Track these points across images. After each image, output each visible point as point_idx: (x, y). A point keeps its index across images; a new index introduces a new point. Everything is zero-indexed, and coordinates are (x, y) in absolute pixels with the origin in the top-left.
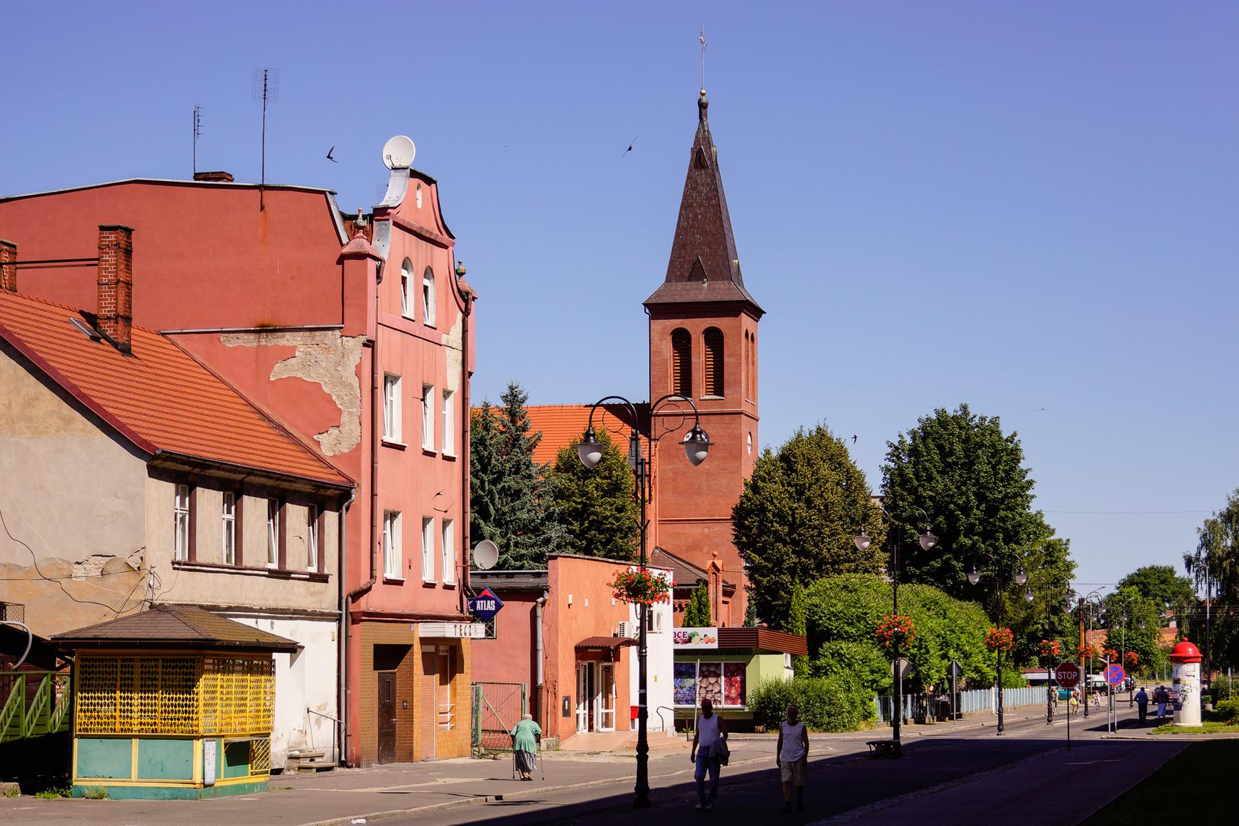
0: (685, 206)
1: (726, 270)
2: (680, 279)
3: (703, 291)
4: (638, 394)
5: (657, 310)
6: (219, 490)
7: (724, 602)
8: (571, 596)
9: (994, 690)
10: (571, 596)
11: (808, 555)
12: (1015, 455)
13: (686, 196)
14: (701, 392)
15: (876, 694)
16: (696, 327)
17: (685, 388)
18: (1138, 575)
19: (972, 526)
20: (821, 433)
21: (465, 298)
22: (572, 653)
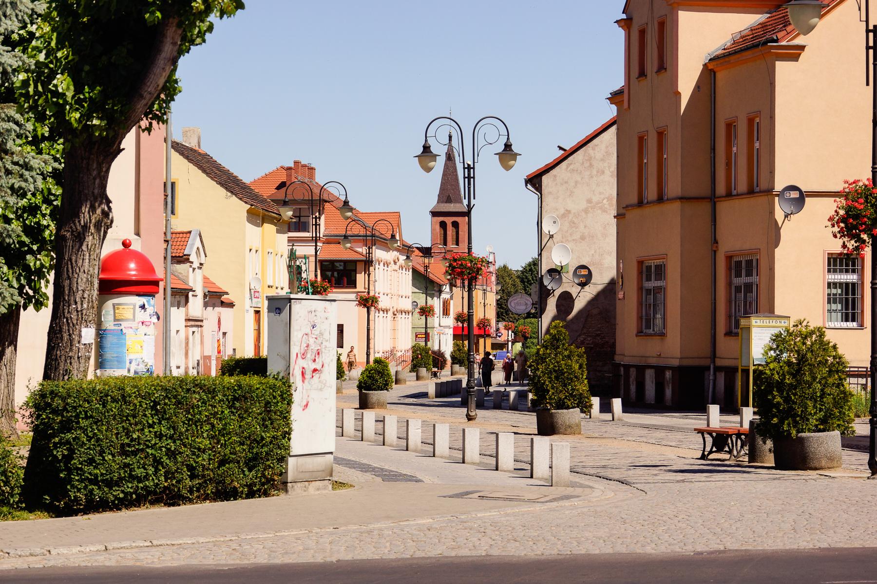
0: (444, 175)
2: (442, 202)
4: (427, 244)
5: (434, 214)
6: (872, 363)
7: (508, 154)
9: (505, 382)
11: (503, 308)
13: (444, 171)
14: (451, 246)
15: (170, 441)
16: (449, 220)
17: (445, 243)
18: (106, 214)
20: (505, 267)
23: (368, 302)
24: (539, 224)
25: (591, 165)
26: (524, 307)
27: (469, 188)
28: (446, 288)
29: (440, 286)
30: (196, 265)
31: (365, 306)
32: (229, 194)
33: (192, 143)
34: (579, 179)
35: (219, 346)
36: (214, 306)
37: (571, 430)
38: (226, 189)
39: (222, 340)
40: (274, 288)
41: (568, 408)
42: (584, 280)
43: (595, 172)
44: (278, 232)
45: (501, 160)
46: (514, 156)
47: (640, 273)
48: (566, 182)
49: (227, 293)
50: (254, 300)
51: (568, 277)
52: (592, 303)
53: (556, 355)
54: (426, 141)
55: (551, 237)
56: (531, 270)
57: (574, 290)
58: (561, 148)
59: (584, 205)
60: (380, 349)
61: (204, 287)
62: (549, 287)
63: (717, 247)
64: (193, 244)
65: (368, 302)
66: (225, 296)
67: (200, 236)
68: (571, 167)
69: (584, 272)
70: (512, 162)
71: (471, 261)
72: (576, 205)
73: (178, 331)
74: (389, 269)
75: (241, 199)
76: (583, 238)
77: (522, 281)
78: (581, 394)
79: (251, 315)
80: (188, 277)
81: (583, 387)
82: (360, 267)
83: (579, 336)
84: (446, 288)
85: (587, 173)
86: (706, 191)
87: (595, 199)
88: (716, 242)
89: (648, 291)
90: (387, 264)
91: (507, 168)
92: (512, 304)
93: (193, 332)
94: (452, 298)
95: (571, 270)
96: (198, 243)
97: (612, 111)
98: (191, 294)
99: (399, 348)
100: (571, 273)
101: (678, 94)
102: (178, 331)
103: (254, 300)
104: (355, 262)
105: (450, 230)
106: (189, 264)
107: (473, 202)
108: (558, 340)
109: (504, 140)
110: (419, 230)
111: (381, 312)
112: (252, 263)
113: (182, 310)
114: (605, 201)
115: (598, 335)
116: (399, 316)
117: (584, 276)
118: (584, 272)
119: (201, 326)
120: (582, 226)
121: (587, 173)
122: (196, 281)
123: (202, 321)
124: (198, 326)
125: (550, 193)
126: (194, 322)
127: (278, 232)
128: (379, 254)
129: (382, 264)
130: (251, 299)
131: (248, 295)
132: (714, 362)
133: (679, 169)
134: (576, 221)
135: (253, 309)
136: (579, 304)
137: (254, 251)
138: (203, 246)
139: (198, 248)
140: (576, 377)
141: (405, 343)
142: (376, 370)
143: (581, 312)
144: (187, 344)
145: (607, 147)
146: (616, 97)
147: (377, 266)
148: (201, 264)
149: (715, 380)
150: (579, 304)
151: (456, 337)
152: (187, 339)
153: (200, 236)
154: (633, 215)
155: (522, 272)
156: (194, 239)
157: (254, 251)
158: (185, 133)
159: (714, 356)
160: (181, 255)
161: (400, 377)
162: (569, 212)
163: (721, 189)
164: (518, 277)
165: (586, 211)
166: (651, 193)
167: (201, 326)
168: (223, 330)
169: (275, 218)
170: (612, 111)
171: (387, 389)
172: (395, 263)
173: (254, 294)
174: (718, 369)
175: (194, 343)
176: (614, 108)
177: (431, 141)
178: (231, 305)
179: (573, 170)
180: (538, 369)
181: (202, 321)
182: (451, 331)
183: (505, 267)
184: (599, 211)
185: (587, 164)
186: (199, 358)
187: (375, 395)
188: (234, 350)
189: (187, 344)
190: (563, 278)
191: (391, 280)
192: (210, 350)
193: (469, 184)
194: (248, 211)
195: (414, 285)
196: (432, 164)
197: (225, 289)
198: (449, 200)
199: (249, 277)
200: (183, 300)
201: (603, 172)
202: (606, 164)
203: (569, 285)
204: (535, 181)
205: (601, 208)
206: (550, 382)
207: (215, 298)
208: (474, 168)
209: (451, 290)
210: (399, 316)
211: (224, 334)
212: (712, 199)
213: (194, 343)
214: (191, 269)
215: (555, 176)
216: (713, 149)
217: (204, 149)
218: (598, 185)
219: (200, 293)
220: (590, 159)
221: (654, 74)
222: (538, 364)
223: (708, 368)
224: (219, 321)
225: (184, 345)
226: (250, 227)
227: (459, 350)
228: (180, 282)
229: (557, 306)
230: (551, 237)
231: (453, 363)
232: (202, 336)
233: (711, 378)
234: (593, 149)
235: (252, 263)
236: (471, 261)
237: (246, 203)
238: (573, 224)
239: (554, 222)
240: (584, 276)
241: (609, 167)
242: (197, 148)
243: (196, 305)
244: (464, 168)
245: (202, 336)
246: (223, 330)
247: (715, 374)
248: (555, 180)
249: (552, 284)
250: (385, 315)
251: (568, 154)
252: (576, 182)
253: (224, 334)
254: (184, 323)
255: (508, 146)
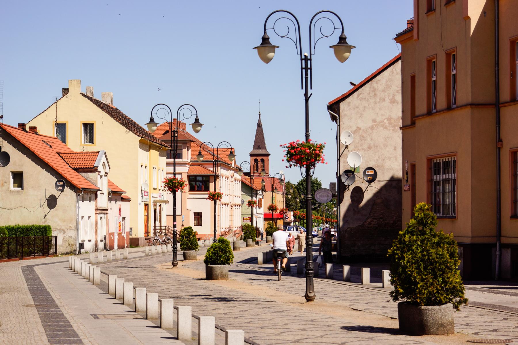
1: (265, 148)
3: (260, 152)
5: (252, 155)
7: (342, 46)
8: (335, 253)
10: (335, 253)
12: (320, 184)
13: (257, 133)
14: (260, 170)
16: (259, 158)
17: (257, 170)
19: (320, 215)
21: (298, 341)
22: (437, 11)
23: (215, 197)
24: (338, 138)
25: (375, 95)
26: (326, 198)
27: (306, 78)
28: (260, 192)
29: (257, 191)
30: (103, 173)
31: (213, 199)
32: (128, 130)
33: (108, 102)
34: (367, 105)
35: (120, 226)
36: (116, 201)
37: (445, 329)
38: (126, 127)
39: (122, 223)
40: (158, 190)
41: (440, 303)
42: (371, 178)
43: (378, 100)
44: (160, 155)
45: (336, 53)
46: (349, 48)
47: (430, 168)
48: (357, 107)
49: (125, 193)
50: (144, 197)
51: (359, 175)
52: (377, 195)
53: (422, 241)
54: (265, 32)
55: (347, 147)
56: (302, 184)
57: (364, 186)
58: (352, 84)
59: (370, 124)
60: (224, 224)
61: (109, 188)
62: (346, 184)
63: (502, 145)
64: (100, 160)
65: (215, 197)
66: (124, 194)
67: (106, 155)
68: (361, 96)
69: (371, 172)
70: (347, 54)
71: (310, 148)
72: (365, 123)
73: (89, 217)
74: (228, 180)
75: (135, 133)
76: (370, 148)
77: (298, 190)
78: (454, 287)
79: (142, 207)
80: (96, 181)
81: (456, 279)
82: (212, 179)
83: (368, 218)
84: (260, 192)
85: (373, 100)
86: (490, 98)
87: (378, 119)
88: (500, 140)
89: (437, 183)
90: (227, 178)
91: (342, 59)
92: (318, 196)
93: (101, 218)
94: (263, 197)
95: (362, 171)
96: (104, 159)
97: (397, 49)
98: (99, 192)
99: (234, 226)
100: (361, 174)
101: (468, 19)
102: (89, 217)
103: (144, 197)
104: (208, 176)
105: (260, 164)
106: (97, 173)
107: (310, 92)
108: (425, 225)
109: (338, 33)
110: (243, 160)
111: (224, 205)
112: (143, 175)
113: (93, 203)
114: (386, 121)
115: (381, 218)
116: (234, 207)
117: (371, 175)
118: (371, 172)
119: (107, 214)
120: (369, 139)
121: (373, 100)
122: (103, 185)
123: (107, 210)
124: (104, 214)
125: (345, 115)
126: (102, 211)
127: (160, 155)
128: (221, 171)
129: (224, 177)
130: (142, 196)
131: (140, 194)
132: (500, 241)
133: (469, 80)
134: (364, 135)
135: (144, 203)
136: (367, 196)
137: (144, 166)
138: (108, 162)
139: (104, 163)
140: (447, 267)
141: (238, 223)
142: (219, 248)
143: (369, 201)
144: (96, 225)
145: (387, 81)
146: (400, 38)
147: (221, 179)
148: (106, 173)
149: (500, 255)
150: (367, 196)
151: (265, 219)
152: (96, 222)
153: (106, 155)
154: (409, 131)
155: (298, 185)
156: (101, 157)
157: (144, 166)
158: (103, 96)
159: (499, 234)
160: (92, 167)
161: (236, 245)
162: (359, 129)
163: (505, 95)
164: (295, 188)
165: (372, 128)
166: (441, 102)
167: (107, 214)
168: (122, 216)
169: (159, 147)
170: (397, 49)
171: (229, 264)
172: (232, 177)
173: (144, 193)
174: (504, 246)
175: (101, 225)
176: (399, 46)
177: (269, 33)
178: (128, 200)
179: (362, 98)
180: (403, 258)
181: (107, 210)
182: (262, 216)
183: (289, 182)
184: (382, 128)
185: (372, 94)
186: (105, 235)
187: (219, 269)
188: (131, 229)
189: (96, 225)
190: (356, 177)
191: (229, 186)
192: (114, 229)
193: (306, 74)
194: (140, 141)
195: (242, 191)
196: (271, 55)
197: (123, 189)
198: (259, 148)
199: (141, 183)
200: (93, 196)
201: (384, 100)
202: (386, 94)
203: (360, 182)
204: (335, 106)
205: (383, 126)
206: (418, 274)
207: (116, 195)
208: (310, 60)
209: (262, 193)
210: (234, 207)
211: (124, 218)
212: (497, 105)
213: (101, 225)
214: (99, 177)
215: (349, 103)
216: (497, 64)
217: (115, 106)
218: (380, 109)
219: (105, 191)
220: (374, 90)
221: (443, 7)
222: (402, 252)
223: (495, 245)
224: (120, 210)
225: (94, 226)
226: (141, 151)
227: (271, 227)
228: (91, 184)
229: (352, 197)
230: (347, 147)
231: (267, 235)
232: (107, 220)
233: (498, 253)
234: (377, 83)
235: (143, 175)
236: (310, 148)
237: (138, 136)
238: (362, 138)
239: (349, 136)
240: (371, 175)
241: (389, 96)
242: (111, 105)
243: (103, 200)
244: (302, 59)
245: (107, 220)
246: (122, 216)
247: (500, 250)
248: (349, 106)
249: (348, 181)
250: (226, 207)
251: (357, 88)
252: (365, 107)
253: (124, 218)
254: (94, 212)
255: (342, 39)
